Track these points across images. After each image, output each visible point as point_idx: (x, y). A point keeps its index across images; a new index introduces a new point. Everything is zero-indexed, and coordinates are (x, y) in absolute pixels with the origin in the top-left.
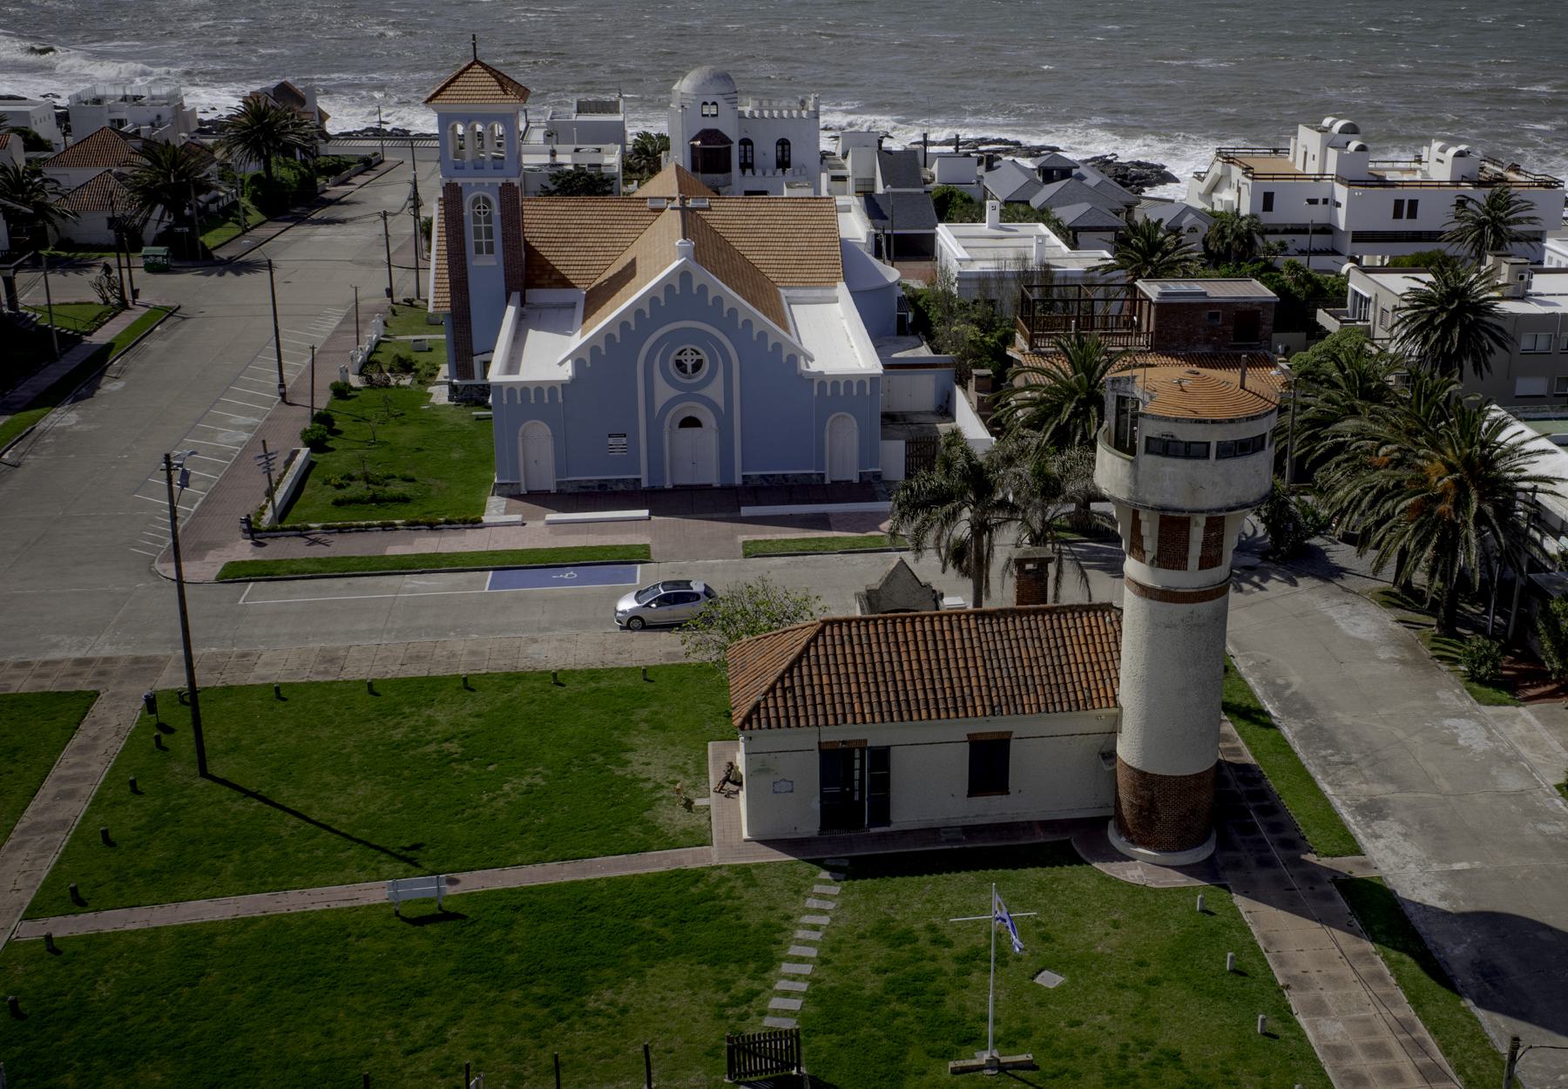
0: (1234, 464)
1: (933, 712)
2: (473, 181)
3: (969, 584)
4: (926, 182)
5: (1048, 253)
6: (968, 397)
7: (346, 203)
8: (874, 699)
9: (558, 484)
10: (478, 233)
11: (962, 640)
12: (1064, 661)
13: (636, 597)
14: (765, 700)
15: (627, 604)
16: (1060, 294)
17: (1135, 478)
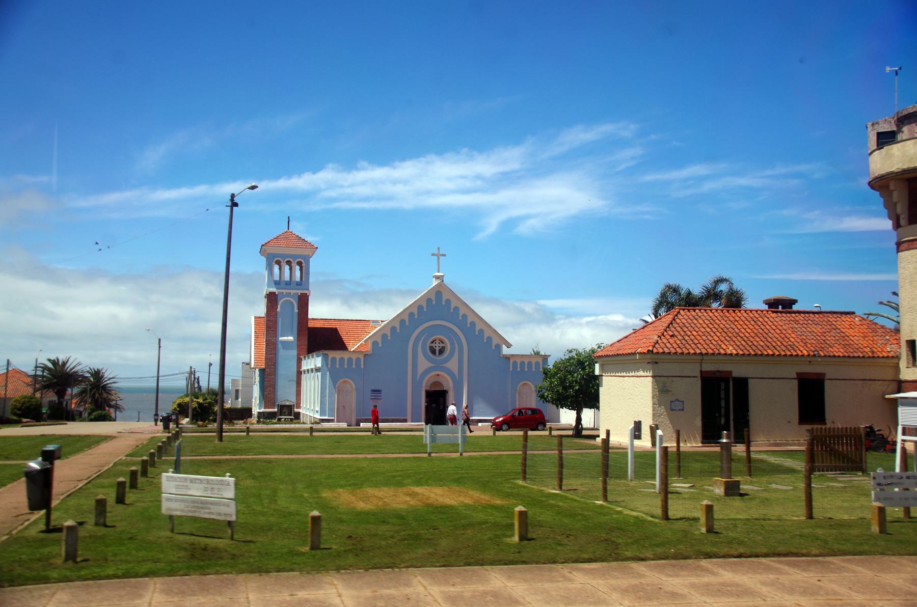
2: (285, 291)
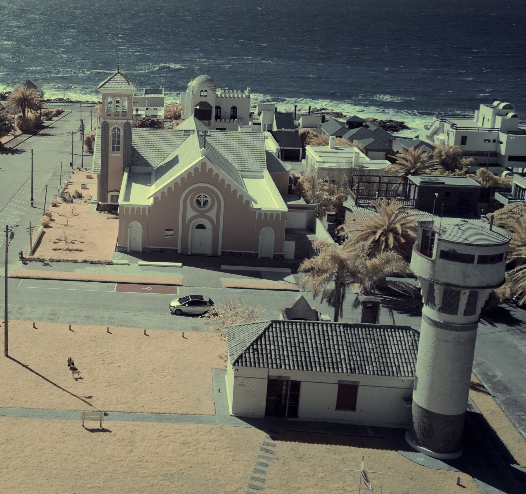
0: (487, 267)
1: (323, 368)
2: (114, 121)
3: (333, 310)
4: (297, 127)
5: (361, 160)
6: (323, 224)
7: (52, 128)
8: (295, 359)
9: (143, 249)
10: (114, 142)
11: (337, 336)
12: (386, 351)
13: (179, 301)
14: (245, 353)
15: (175, 303)
16: (366, 179)
17: (433, 269)
